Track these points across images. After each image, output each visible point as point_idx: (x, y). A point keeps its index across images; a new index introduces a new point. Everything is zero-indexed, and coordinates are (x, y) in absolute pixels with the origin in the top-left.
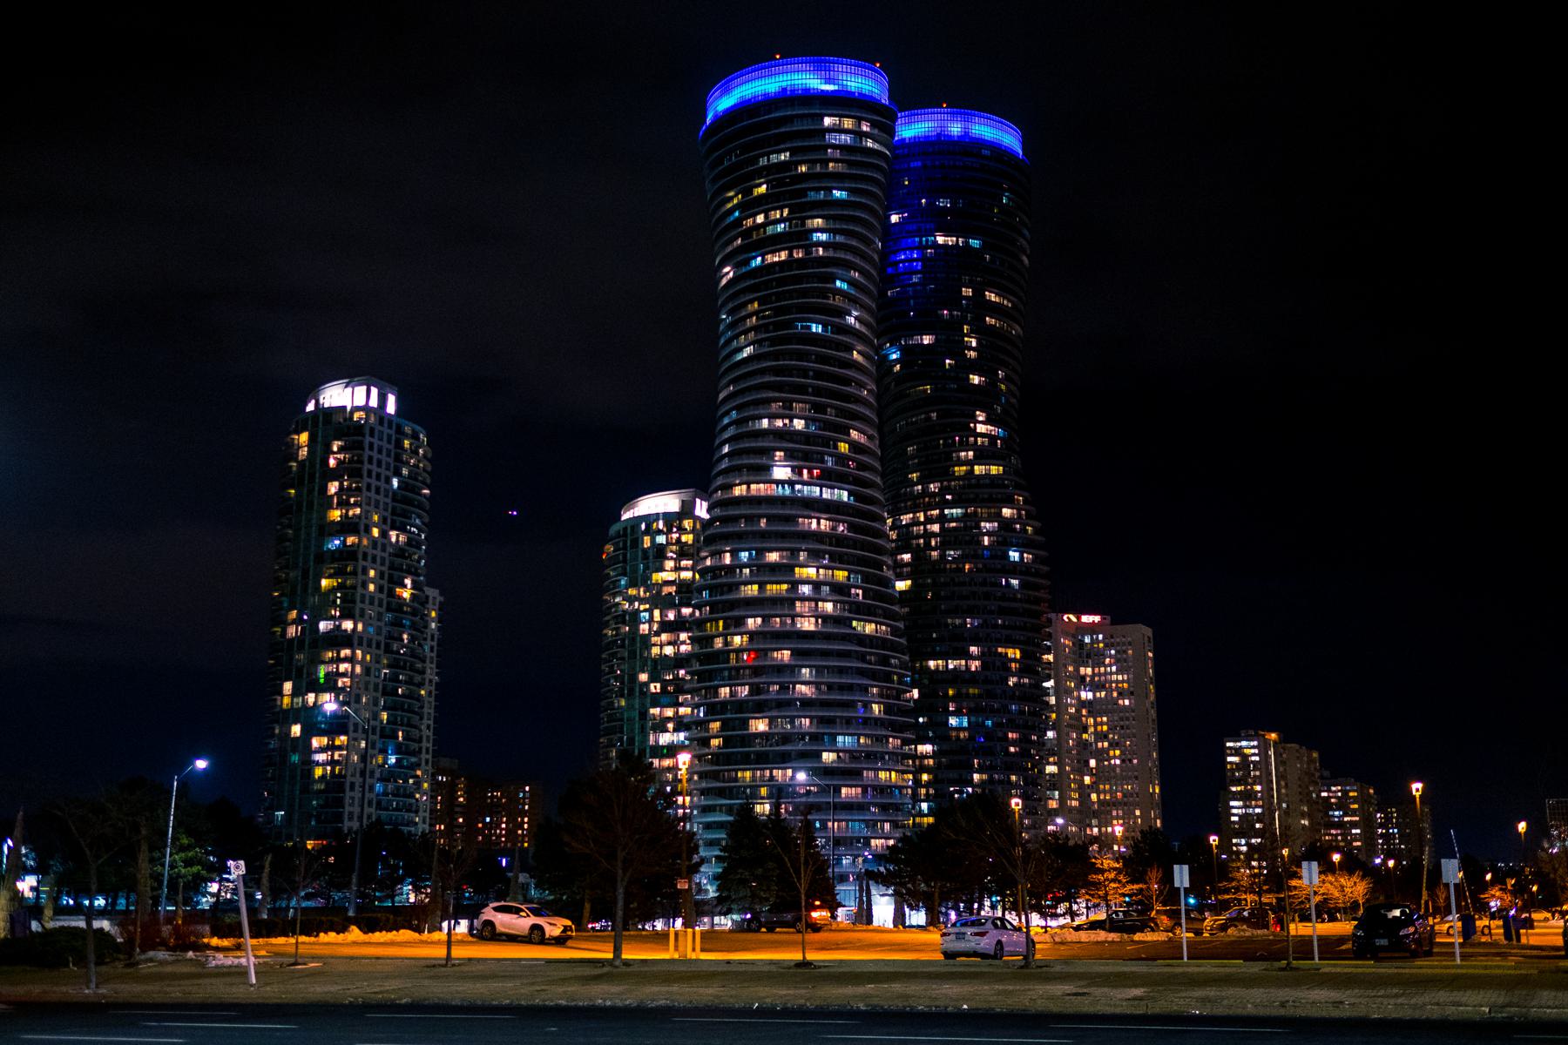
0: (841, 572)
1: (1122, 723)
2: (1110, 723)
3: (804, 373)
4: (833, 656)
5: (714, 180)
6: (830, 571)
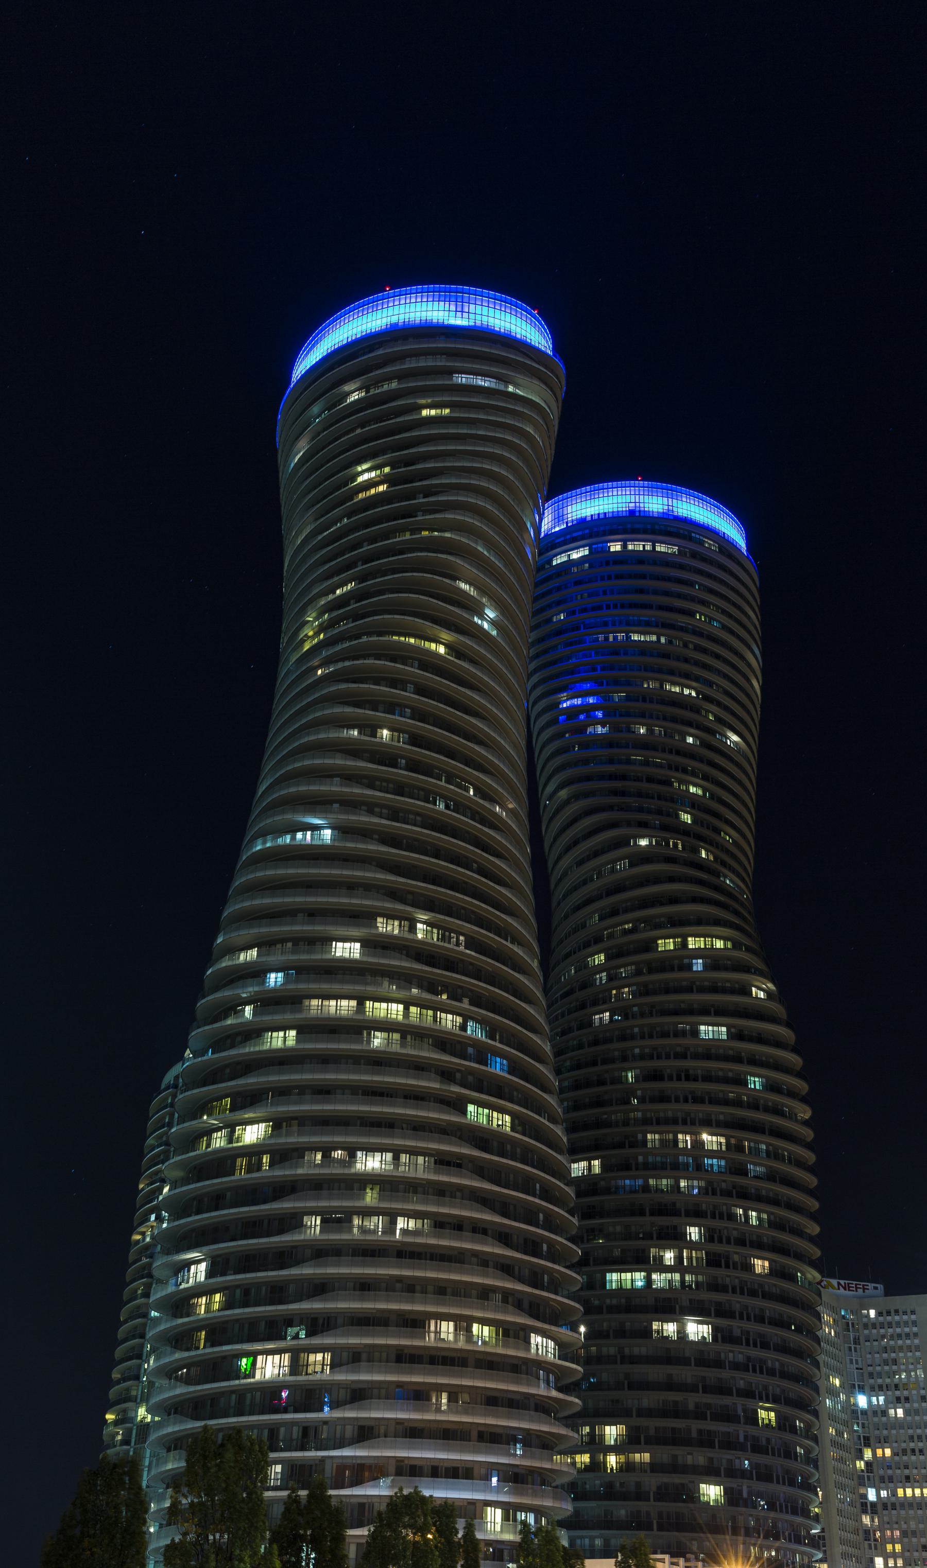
0: (450, 1017)
1: (912, 1445)
2: (907, 1554)
3: (396, 682)
4: (424, 1291)
5: (179, 1208)
6: (430, 1013)
